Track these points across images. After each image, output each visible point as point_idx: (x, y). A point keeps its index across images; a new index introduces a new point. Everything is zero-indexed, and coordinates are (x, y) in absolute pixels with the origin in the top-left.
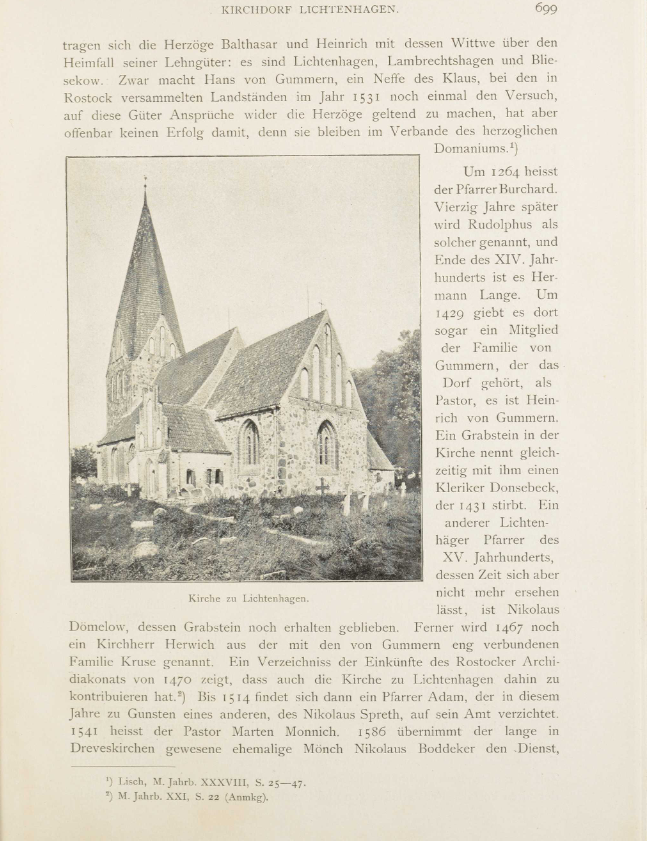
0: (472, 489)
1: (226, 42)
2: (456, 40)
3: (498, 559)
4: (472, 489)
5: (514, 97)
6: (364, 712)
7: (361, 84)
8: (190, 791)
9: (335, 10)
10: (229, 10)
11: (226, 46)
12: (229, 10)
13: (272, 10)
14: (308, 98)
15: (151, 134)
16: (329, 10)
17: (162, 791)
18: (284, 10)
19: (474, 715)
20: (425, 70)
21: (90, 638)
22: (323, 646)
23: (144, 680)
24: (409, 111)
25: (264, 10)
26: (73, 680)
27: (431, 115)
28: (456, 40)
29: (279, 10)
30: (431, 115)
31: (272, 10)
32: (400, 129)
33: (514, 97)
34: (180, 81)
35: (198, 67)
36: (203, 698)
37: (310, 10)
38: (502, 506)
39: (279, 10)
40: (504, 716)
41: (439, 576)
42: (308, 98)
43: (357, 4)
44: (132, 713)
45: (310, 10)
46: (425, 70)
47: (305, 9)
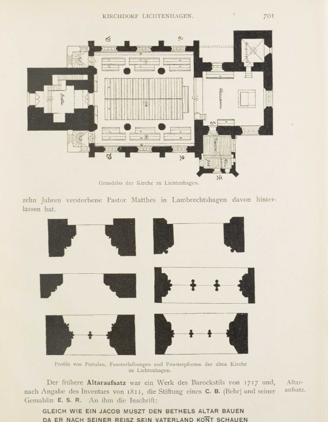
1: (194, 381)
6: (161, 390)
8: (190, 386)
9: (161, 16)
10: (106, 16)
11: (194, 383)
12: (106, 16)
13: (129, 16)
15: (94, 392)
17: (184, 388)
18: (135, 16)
23: (234, 383)
26: (149, 392)
28: (159, 381)
29: (132, 16)
31: (129, 16)
32: (164, 382)
34: (33, 392)
37: (148, 16)
38: (218, 383)
39: (132, 16)
40: (91, 393)
41: (71, 392)
43: (172, 14)
44: (27, 400)
45: (148, 16)
47: (145, 16)
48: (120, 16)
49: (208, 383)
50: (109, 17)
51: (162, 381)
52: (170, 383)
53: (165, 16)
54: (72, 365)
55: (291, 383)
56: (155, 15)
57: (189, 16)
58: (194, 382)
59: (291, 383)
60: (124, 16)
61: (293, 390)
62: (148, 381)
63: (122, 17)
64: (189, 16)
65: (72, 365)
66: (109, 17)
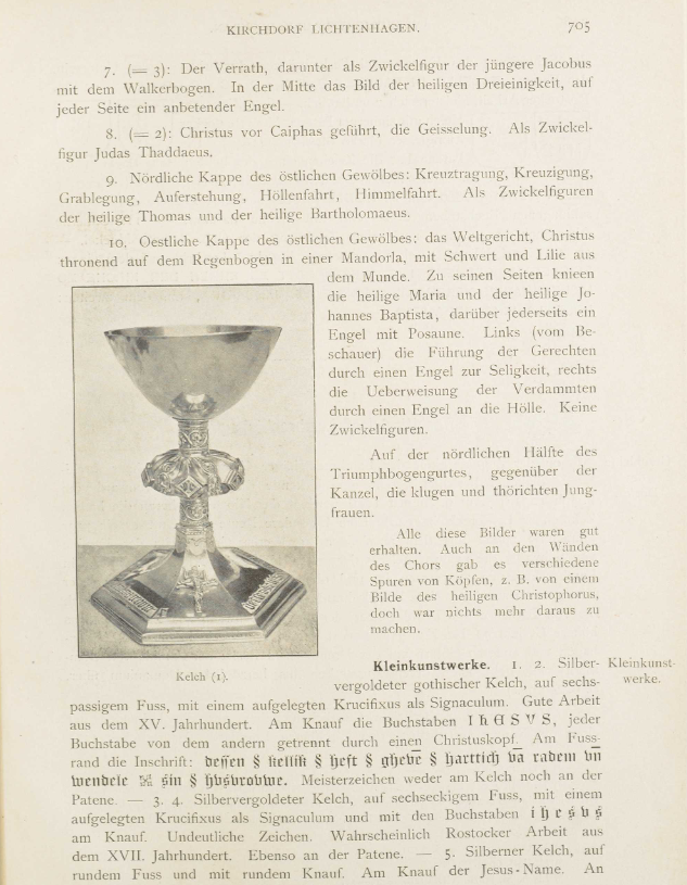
0: (529, 371)
2: (336, 833)
3: (178, 857)
4: (529, 371)
5: (223, 70)
6: (198, 796)
7: (240, 711)
9: (351, 29)
11: (386, 317)
13: (282, 30)
14: (240, 707)
16: (344, 29)
17: (470, 77)
18: (295, 30)
19: (373, 874)
20: (424, 807)
21: (95, 718)
22: (76, 858)
24: (93, 759)
25: (273, 30)
27: (467, 372)
28: (336, 833)
29: (289, 30)
30: (467, 372)
31: (282, 30)
33: (223, 70)
35: (255, 805)
36: (388, 724)
37: (323, 29)
39: (289, 30)
42: (240, 707)
45: (323, 29)
46: (424, 807)
47: (318, 29)
48: (265, 30)
49: (488, 834)
50: (241, 32)
51: (341, 833)
52: (643, 680)
53: (406, 27)
54: (237, 134)
55: (406, 536)
56: (338, 27)
57: (412, 28)
58: (547, 64)
59: (406, 536)
60: (273, 30)
61: (259, 875)
62: (395, 739)
63: (268, 31)
64: (412, 28)
65: (237, 134)
66: (241, 32)
